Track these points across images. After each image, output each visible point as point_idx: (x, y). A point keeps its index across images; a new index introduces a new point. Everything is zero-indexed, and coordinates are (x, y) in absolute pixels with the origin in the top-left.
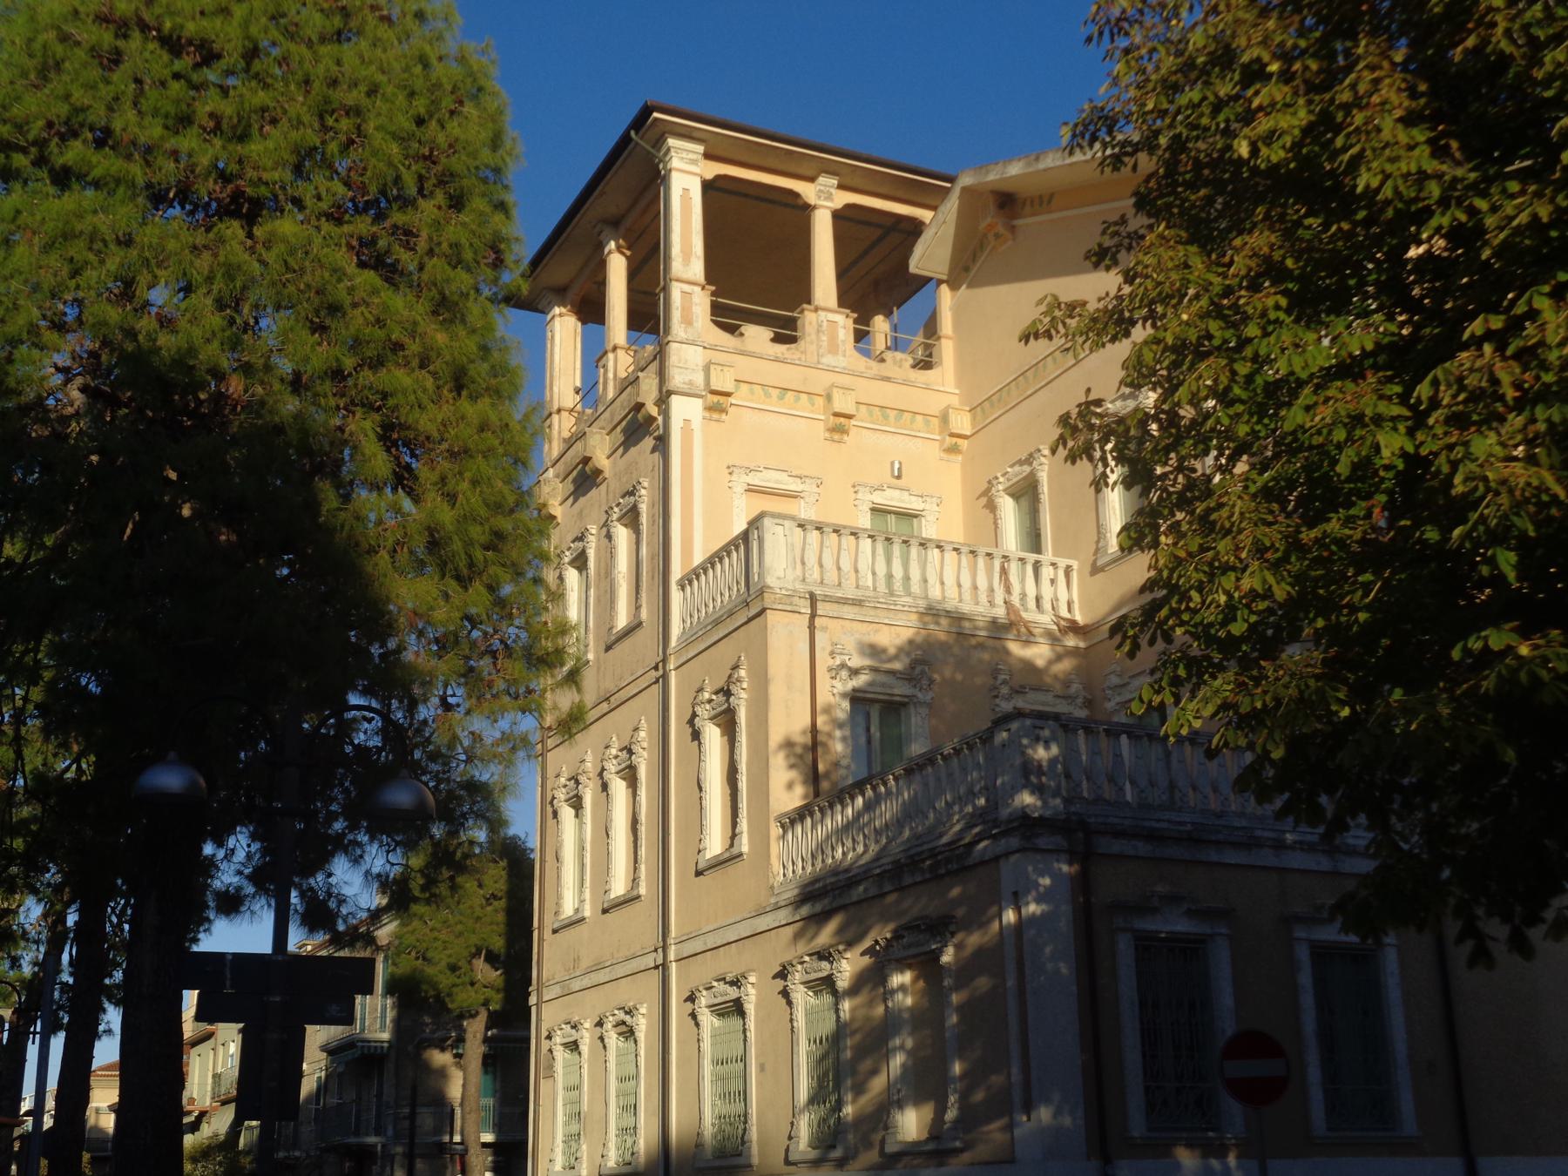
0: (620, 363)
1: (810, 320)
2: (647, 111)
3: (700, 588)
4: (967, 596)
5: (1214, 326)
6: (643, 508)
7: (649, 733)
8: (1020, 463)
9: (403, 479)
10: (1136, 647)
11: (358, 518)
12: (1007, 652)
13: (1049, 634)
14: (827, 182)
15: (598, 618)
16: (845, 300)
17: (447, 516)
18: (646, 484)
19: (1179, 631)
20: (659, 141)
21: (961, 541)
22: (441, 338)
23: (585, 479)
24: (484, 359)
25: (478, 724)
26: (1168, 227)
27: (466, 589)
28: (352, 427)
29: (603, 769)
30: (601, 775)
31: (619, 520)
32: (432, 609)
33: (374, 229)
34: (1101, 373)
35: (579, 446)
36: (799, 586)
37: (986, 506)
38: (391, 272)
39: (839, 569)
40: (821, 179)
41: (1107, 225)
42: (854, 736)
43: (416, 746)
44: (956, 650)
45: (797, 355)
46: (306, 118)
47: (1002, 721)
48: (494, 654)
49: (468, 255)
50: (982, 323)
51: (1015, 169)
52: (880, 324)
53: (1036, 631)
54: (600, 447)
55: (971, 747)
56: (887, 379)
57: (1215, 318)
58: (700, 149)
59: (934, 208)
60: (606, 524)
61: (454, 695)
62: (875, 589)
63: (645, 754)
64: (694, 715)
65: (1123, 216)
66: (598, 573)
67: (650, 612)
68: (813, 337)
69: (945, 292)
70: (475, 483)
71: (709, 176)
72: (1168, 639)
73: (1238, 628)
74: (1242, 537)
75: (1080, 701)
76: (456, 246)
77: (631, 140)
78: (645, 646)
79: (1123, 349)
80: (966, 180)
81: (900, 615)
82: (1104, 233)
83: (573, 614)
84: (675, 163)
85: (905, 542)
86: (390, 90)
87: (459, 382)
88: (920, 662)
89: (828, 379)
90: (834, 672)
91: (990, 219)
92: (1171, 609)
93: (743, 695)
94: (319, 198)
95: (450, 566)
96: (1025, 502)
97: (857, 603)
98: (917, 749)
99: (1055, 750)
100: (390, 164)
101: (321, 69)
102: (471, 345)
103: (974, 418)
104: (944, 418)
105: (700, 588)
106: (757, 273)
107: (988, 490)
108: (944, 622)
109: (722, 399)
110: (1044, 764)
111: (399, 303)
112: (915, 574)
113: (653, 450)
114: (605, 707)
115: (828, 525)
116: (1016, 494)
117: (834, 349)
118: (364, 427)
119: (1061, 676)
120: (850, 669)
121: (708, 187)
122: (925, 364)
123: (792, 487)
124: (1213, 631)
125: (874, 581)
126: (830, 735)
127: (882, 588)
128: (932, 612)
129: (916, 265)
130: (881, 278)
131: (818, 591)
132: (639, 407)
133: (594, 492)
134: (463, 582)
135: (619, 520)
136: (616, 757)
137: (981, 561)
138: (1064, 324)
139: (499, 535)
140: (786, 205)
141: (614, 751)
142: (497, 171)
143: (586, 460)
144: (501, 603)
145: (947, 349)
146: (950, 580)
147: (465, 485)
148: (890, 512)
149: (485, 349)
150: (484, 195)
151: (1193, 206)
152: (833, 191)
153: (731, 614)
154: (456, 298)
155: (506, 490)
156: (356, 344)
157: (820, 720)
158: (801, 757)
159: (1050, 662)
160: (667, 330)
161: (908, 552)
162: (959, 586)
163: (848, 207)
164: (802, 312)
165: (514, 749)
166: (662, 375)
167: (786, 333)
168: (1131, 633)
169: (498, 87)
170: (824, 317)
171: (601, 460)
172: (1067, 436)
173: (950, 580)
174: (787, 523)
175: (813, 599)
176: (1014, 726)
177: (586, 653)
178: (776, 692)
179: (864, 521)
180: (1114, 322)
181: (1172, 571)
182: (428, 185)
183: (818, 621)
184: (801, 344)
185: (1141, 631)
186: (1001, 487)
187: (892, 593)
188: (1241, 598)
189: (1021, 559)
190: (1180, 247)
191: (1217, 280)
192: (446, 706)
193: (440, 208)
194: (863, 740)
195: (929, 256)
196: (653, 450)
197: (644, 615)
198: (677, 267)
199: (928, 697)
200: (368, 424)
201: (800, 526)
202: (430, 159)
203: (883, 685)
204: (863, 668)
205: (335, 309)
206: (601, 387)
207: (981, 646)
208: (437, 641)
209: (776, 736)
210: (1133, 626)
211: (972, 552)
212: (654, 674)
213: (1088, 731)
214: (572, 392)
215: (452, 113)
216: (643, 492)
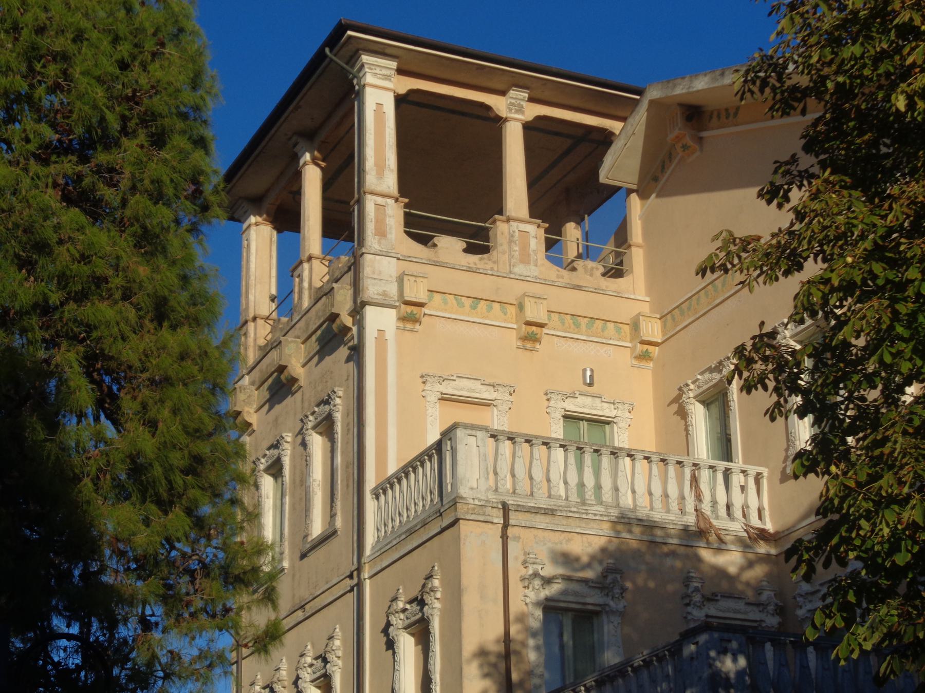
0: (315, 273)
1: (501, 230)
2: (341, 29)
3: (394, 497)
4: (658, 504)
5: (877, 268)
6: (338, 416)
7: (344, 641)
8: (710, 370)
9: (108, 405)
10: (811, 570)
11: (63, 450)
12: (699, 560)
13: (740, 541)
14: (518, 95)
15: (292, 525)
16: (536, 211)
17: (148, 444)
18: (340, 393)
19: (852, 555)
20: (353, 58)
21: (653, 449)
22: (143, 271)
23: (280, 387)
24: (183, 288)
25: (175, 641)
26: (832, 173)
27: (166, 513)
28: (58, 359)
29: (298, 678)
30: (295, 683)
31: (314, 428)
32: (134, 534)
33: (80, 168)
34: (773, 305)
35: (274, 354)
36: (492, 496)
37: (677, 413)
38: (94, 209)
39: (531, 478)
40: (512, 93)
41: (779, 164)
42: (547, 643)
43: (115, 663)
44: (648, 558)
45: (490, 265)
46: (14, 65)
47: (689, 635)
48: (191, 573)
49: (169, 191)
50: (672, 230)
51: (701, 84)
52: (572, 232)
53: (728, 538)
54: (295, 357)
55: (661, 659)
56: (578, 288)
57: (877, 261)
58: (394, 64)
59: (623, 119)
60: (301, 432)
61: (153, 615)
62: (567, 499)
63: (340, 663)
64: (388, 624)
65: (794, 156)
66: (293, 481)
67: (345, 521)
68: (505, 247)
69: (635, 201)
70: (175, 411)
71: (402, 91)
72: (843, 562)
73: (902, 559)
74: (904, 472)
75: (771, 608)
76: (157, 182)
77: (326, 56)
78: (339, 553)
79: (792, 284)
80: (654, 93)
81: (592, 524)
82: (776, 172)
83: (269, 534)
84: (369, 79)
85: (596, 451)
86: (95, 35)
87: (161, 312)
88: (613, 570)
89: (520, 288)
90: (527, 581)
91: (678, 130)
92: (841, 537)
93: (437, 605)
94: (28, 141)
95: (151, 491)
96: (715, 408)
97: (549, 512)
98: (611, 657)
99: (742, 662)
100: (95, 107)
101: (29, 17)
102: (171, 276)
103: (664, 326)
104: (635, 326)
105: (394, 497)
106: (450, 188)
107: (679, 397)
108: (637, 530)
109: (415, 310)
110: (732, 675)
111: (102, 238)
112: (606, 482)
113: (348, 360)
114: (300, 615)
115: (520, 435)
116: (706, 403)
117: (525, 258)
118: (68, 358)
119: (753, 582)
120: (543, 578)
121: (401, 101)
122: (616, 272)
123: (485, 396)
124: (880, 560)
125: (566, 490)
126: (524, 644)
127: (574, 498)
128: (625, 521)
129: (605, 175)
130: (571, 186)
131: (510, 501)
132: (334, 317)
133: (289, 400)
134: (165, 506)
135: (314, 428)
136: (311, 665)
137: (672, 470)
138: (739, 257)
139: (198, 459)
140: (478, 117)
141: (309, 660)
142: (197, 108)
143: (282, 369)
144: (200, 523)
145: (637, 258)
146: (641, 488)
147: (166, 413)
148: (582, 419)
149: (185, 279)
150: (184, 132)
151: (859, 149)
152: (524, 104)
153: (425, 524)
154: (157, 230)
155: (205, 416)
156: (63, 279)
157: (513, 630)
158: (495, 666)
159: (743, 569)
160: (361, 243)
161: (600, 462)
162: (650, 494)
163: (539, 118)
164: (494, 222)
165: (210, 666)
166: (356, 286)
167: (479, 243)
168: (806, 557)
169: (197, 27)
170: (518, 226)
171: (297, 368)
172: (742, 367)
173: (641, 488)
174: (479, 434)
175: (505, 509)
176: (703, 638)
177: (281, 561)
178: (470, 601)
179: (557, 430)
180: (783, 257)
181: (842, 500)
182: (132, 124)
183: (510, 531)
184: (494, 254)
185: (816, 554)
186: (691, 394)
187: (584, 503)
188: (904, 530)
189: (711, 467)
190: (845, 192)
191: (879, 222)
192: (146, 625)
193: (142, 147)
194: (556, 649)
195: (619, 165)
196: (348, 360)
197: (339, 523)
198: (371, 180)
199: (621, 605)
200: (72, 356)
201: (493, 436)
202: (133, 99)
203: (576, 594)
204: (555, 577)
205: (43, 247)
206: (296, 296)
207: (673, 554)
208: (136, 560)
209: (469, 646)
210: (808, 550)
211: (663, 460)
212: (349, 583)
213: (776, 643)
214: (268, 300)
215: (154, 55)
216: (338, 401)
